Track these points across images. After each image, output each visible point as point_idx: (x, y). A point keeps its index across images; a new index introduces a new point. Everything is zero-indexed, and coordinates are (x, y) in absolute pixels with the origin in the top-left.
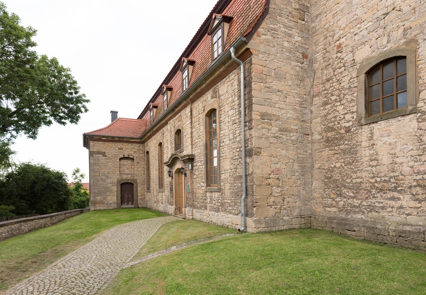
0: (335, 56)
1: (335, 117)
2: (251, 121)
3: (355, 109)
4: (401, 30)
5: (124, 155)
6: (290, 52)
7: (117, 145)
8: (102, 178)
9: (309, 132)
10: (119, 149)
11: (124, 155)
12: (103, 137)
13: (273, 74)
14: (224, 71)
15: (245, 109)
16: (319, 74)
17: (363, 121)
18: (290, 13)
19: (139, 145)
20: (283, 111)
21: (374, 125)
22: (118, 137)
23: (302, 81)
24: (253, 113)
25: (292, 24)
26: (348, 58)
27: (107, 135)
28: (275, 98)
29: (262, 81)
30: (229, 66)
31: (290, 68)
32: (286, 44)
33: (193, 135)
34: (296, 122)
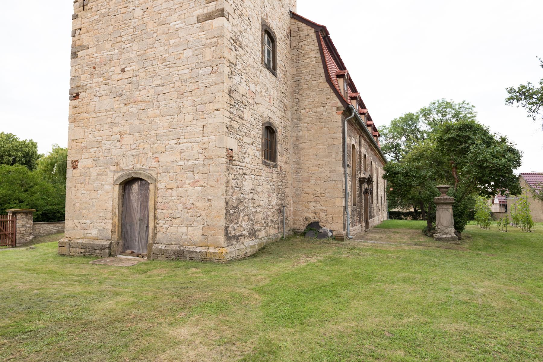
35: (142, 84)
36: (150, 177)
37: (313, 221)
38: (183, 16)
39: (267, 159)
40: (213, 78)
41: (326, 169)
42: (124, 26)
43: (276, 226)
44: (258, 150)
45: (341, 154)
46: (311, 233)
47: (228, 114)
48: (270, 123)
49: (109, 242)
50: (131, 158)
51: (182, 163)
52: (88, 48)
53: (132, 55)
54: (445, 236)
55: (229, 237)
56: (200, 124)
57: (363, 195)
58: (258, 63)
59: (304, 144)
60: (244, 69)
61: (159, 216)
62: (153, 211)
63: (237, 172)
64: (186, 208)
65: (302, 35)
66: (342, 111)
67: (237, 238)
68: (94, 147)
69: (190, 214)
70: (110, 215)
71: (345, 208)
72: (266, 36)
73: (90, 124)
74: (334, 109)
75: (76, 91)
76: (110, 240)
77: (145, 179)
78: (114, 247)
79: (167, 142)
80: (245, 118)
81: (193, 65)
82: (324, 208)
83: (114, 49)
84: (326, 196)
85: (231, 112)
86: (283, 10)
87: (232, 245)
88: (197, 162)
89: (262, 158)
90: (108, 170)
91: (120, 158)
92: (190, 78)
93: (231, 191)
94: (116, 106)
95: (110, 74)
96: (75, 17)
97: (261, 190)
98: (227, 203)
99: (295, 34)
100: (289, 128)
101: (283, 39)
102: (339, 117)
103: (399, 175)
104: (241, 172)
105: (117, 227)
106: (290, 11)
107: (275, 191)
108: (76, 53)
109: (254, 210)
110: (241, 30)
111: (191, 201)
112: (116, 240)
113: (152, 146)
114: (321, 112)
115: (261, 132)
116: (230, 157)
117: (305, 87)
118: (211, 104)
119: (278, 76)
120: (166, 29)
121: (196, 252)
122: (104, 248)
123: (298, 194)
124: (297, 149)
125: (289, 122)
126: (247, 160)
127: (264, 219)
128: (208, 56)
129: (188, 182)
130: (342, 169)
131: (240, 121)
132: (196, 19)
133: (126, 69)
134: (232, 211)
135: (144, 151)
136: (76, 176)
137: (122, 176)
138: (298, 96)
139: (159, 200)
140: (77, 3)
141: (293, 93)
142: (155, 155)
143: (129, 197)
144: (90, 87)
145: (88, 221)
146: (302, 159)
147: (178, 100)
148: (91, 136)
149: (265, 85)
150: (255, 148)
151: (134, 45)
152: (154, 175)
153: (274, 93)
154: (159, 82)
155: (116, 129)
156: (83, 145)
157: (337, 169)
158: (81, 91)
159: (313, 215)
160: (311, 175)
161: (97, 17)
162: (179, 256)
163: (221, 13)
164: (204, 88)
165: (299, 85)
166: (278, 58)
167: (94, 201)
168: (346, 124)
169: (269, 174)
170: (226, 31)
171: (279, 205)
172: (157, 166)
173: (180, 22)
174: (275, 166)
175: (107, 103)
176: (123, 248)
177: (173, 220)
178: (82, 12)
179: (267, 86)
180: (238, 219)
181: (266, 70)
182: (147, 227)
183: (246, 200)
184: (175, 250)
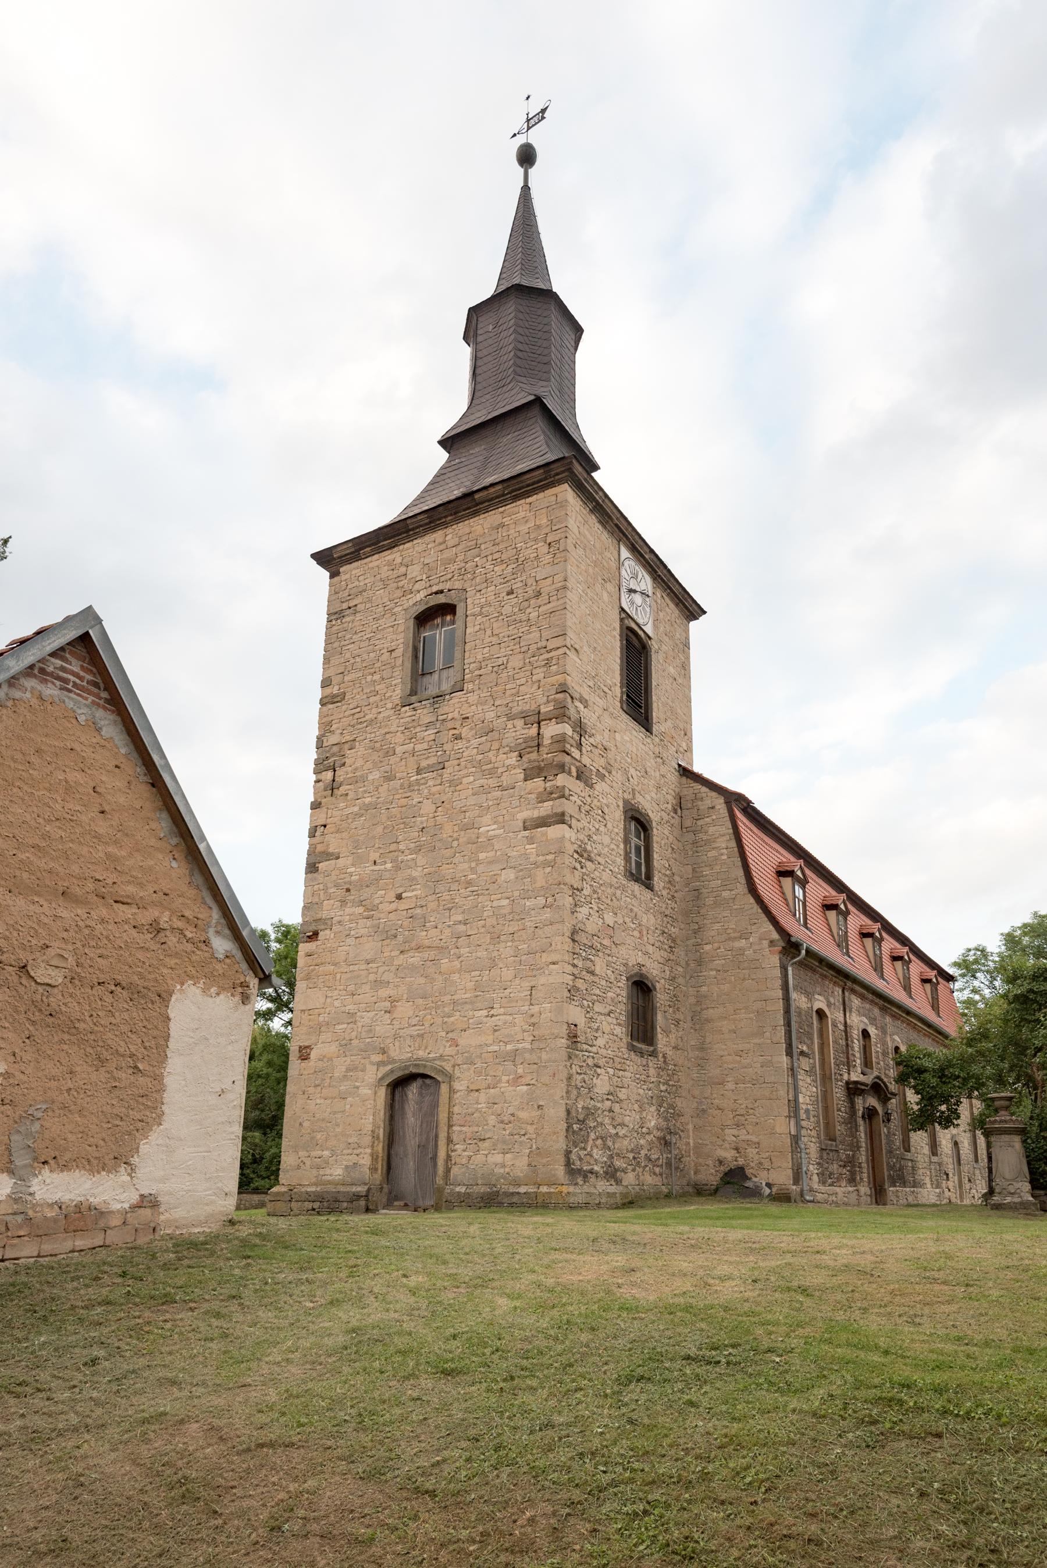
35: (432, 919)
36: (442, 1071)
37: (733, 1165)
38: (501, 819)
39: (638, 1040)
40: (547, 914)
41: (755, 1059)
42: (402, 826)
43: (657, 1170)
44: (620, 1025)
45: (781, 1032)
46: (729, 1188)
47: (569, 969)
48: (642, 975)
49: (366, 1188)
50: (408, 1042)
51: (496, 1048)
52: (338, 858)
53: (415, 874)
54: (1008, 1200)
55: (573, 1172)
56: (526, 984)
57: (860, 1121)
58: (619, 876)
59: (711, 1011)
60: (595, 892)
61: (455, 1138)
62: (446, 1129)
63: (584, 1061)
64: (502, 1122)
65: (701, 808)
66: (780, 948)
67: (586, 1175)
68: (343, 1023)
69: (508, 1132)
70: (367, 1140)
71: (796, 1139)
72: (633, 823)
73: (337, 983)
74: (766, 943)
75: (313, 928)
76: (366, 1184)
77: (432, 1075)
78: (375, 1196)
79: (471, 1013)
80: (597, 972)
81: (516, 893)
82: (754, 1138)
83: (385, 863)
84: (756, 1113)
85: (574, 966)
86: (664, 769)
87: (576, 1184)
88: (521, 1046)
89: (626, 1039)
90: (367, 1061)
91: (389, 1041)
92: (510, 913)
93: (575, 1092)
94: (385, 954)
95: (377, 901)
96: (315, 806)
97: (627, 1097)
98: (568, 1112)
99: (690, 805)
100: (680, 980)
101: (666, 817)
102: (775, 960)
103: (926, 1075)
104: (590, 1062)
105: (380, 1159)
106: (680, 766)
107: (654, 1102)
108: (315, 864)
109: (613, 1131)
110: (590, 833)
111: (511, 1110)
112: (378, 1182)
113: (446, 1019)
114: (742, 949)
115: (624, 993)
116: (573, 1037)
117: (709, 901)
118: (544, 954)
119: (656, 888)
120: (474, 836)
121: (518, 1193)
122: (357, 1197)
123: (703, 1110)
124: (698, 1021)
125: (680, 969)
126: (601, 1042)
127: (632, 1151)
128: (540, 882)
129: (505, 1078)
130: (785, 1059)
131: (588, 977)
132: (521, 825)
133: (404, 895)
134: (578, 1126)
135: (434, 1029)
136: (305, 1072)
137: (392, 1071)
138: (696, 919)
139: (456, 1110)
140: (321, 784)
141: (686, 913)
142: (450, 1035)
143: (403, 1108)
144: (340, 922)
145: (326, 1153)
146: (708, 1040)
147: (491, 947)
148: (337, 1003)
149: (631, 910)
150: (615, 1021)
151: (420, 857)
152: (449, 1068)
153: (649, 920)
154: (460, 918)
155: (384, 993)
156: (321, 1019)
157: (775, 1059)
158: (323, 927)
159: (733, 1153)
160: (726, 1072)
161: (356, 809)
162: (491, 1200)
163: (561, 819)
164: (532, 929)
165: (698, 898)
166: (655, 856)
167: (339, 1116)
168: (790, 972)
169: (641, 1068)
170: (568, 845)
171: (662, 1130)
172: (453, 1053)
173: (495, 826)
174: (653, 1054)
175: (369, 948)
176: (388, 1200)
177: (480, 1144)
178: (329, 798)
179: (635, 909)
180: (586, 1142)
181: (632, 883)
182: (434, 1158)
183: (600, 1112)
184: (484, 1193)
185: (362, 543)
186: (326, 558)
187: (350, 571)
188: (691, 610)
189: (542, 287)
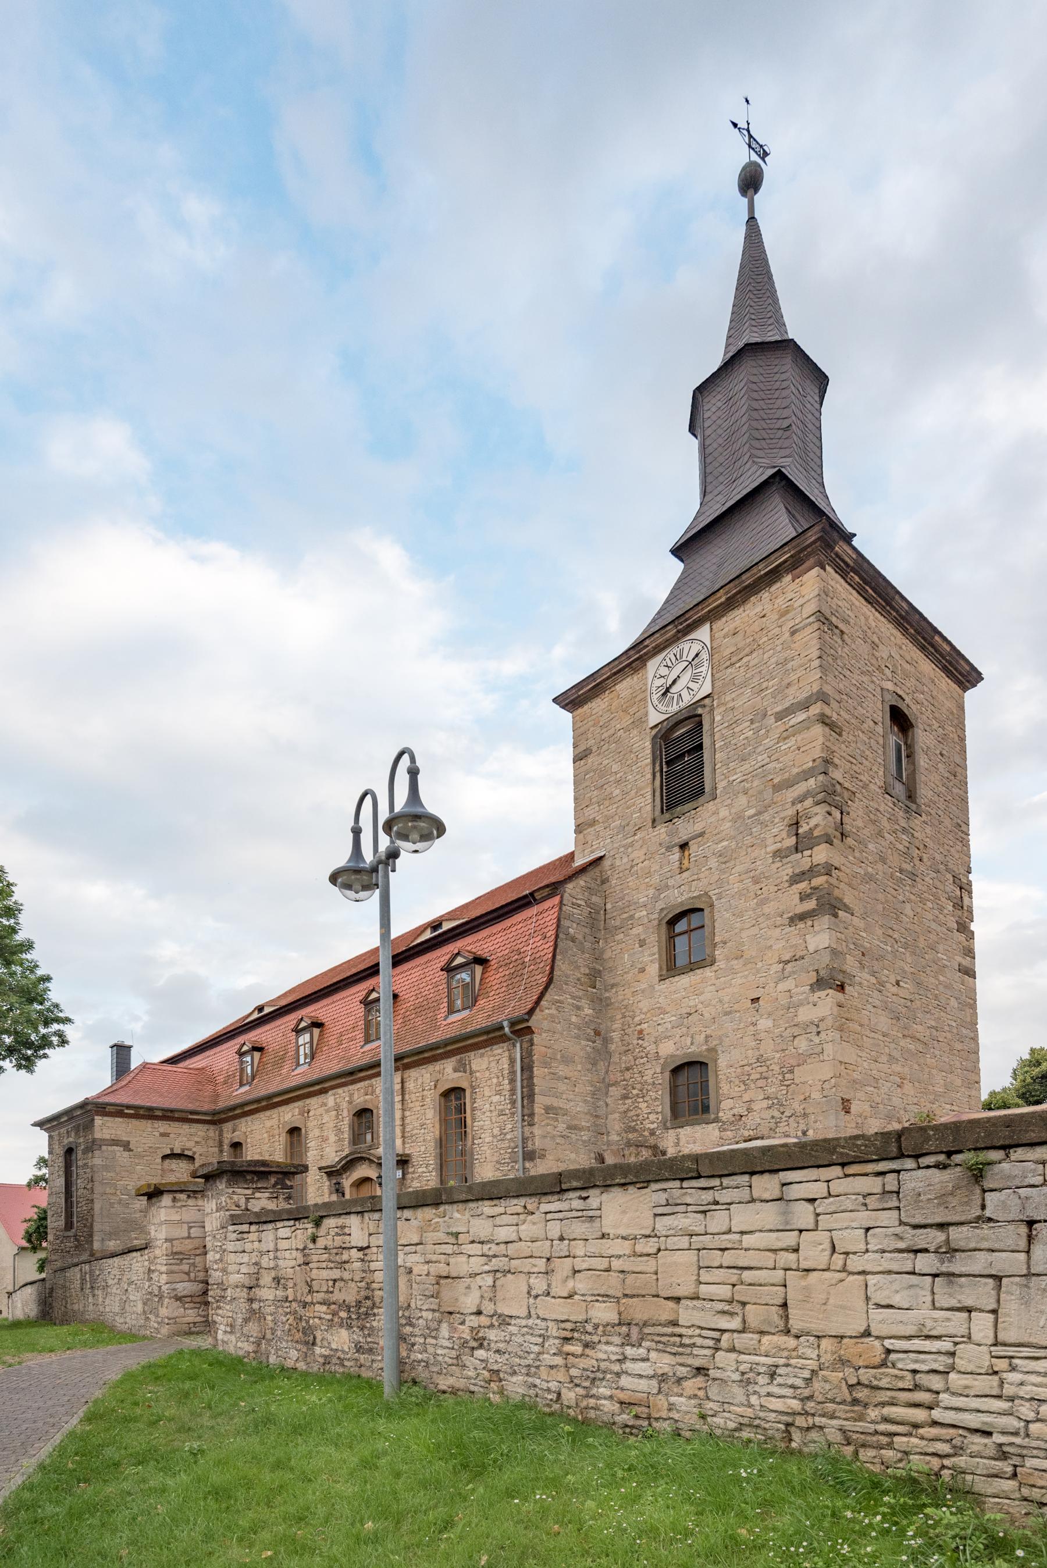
0: (635, 1042)
1: (638, 1115)
2: (532, 1115)
3: (660, 1110)
4: (703, 1036)
5: (172, 1149)
6: (579, 1029)
7: (156, 1125)
8: (120, 1200)
9: (604, 1130)
10: (162, 1135)
11: (172, 1149)
12: (128, 1107)
13: (559, 1057)
14: (486, 1041)
15: (522, 1098)
16: (615, 1058)
17: (669, 1124)
18: (578, 980)
19: (206, 1127)
20: (572, 1104)
21: (680, 1130)
22: (163, 1110)
23: (594, 1064)
24: (536, 1105)
25: (581, 993)
26: (651, 1048)
27: (138, 1102)
28: (562, 1087)
29: (546, 1065)
30: (493, 1038)
31: (580, 1049)
32: (574, 1019)
33: (407, 1121)
34: (588, 1117)
185: (861, 567)
186: (572, 700)
187: (597, 706)
188: (964, 674)
189: (778, 338)
